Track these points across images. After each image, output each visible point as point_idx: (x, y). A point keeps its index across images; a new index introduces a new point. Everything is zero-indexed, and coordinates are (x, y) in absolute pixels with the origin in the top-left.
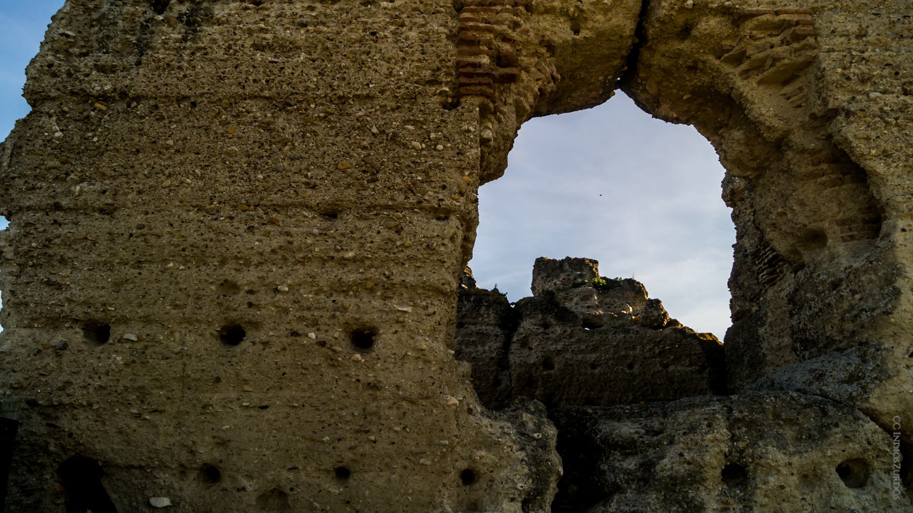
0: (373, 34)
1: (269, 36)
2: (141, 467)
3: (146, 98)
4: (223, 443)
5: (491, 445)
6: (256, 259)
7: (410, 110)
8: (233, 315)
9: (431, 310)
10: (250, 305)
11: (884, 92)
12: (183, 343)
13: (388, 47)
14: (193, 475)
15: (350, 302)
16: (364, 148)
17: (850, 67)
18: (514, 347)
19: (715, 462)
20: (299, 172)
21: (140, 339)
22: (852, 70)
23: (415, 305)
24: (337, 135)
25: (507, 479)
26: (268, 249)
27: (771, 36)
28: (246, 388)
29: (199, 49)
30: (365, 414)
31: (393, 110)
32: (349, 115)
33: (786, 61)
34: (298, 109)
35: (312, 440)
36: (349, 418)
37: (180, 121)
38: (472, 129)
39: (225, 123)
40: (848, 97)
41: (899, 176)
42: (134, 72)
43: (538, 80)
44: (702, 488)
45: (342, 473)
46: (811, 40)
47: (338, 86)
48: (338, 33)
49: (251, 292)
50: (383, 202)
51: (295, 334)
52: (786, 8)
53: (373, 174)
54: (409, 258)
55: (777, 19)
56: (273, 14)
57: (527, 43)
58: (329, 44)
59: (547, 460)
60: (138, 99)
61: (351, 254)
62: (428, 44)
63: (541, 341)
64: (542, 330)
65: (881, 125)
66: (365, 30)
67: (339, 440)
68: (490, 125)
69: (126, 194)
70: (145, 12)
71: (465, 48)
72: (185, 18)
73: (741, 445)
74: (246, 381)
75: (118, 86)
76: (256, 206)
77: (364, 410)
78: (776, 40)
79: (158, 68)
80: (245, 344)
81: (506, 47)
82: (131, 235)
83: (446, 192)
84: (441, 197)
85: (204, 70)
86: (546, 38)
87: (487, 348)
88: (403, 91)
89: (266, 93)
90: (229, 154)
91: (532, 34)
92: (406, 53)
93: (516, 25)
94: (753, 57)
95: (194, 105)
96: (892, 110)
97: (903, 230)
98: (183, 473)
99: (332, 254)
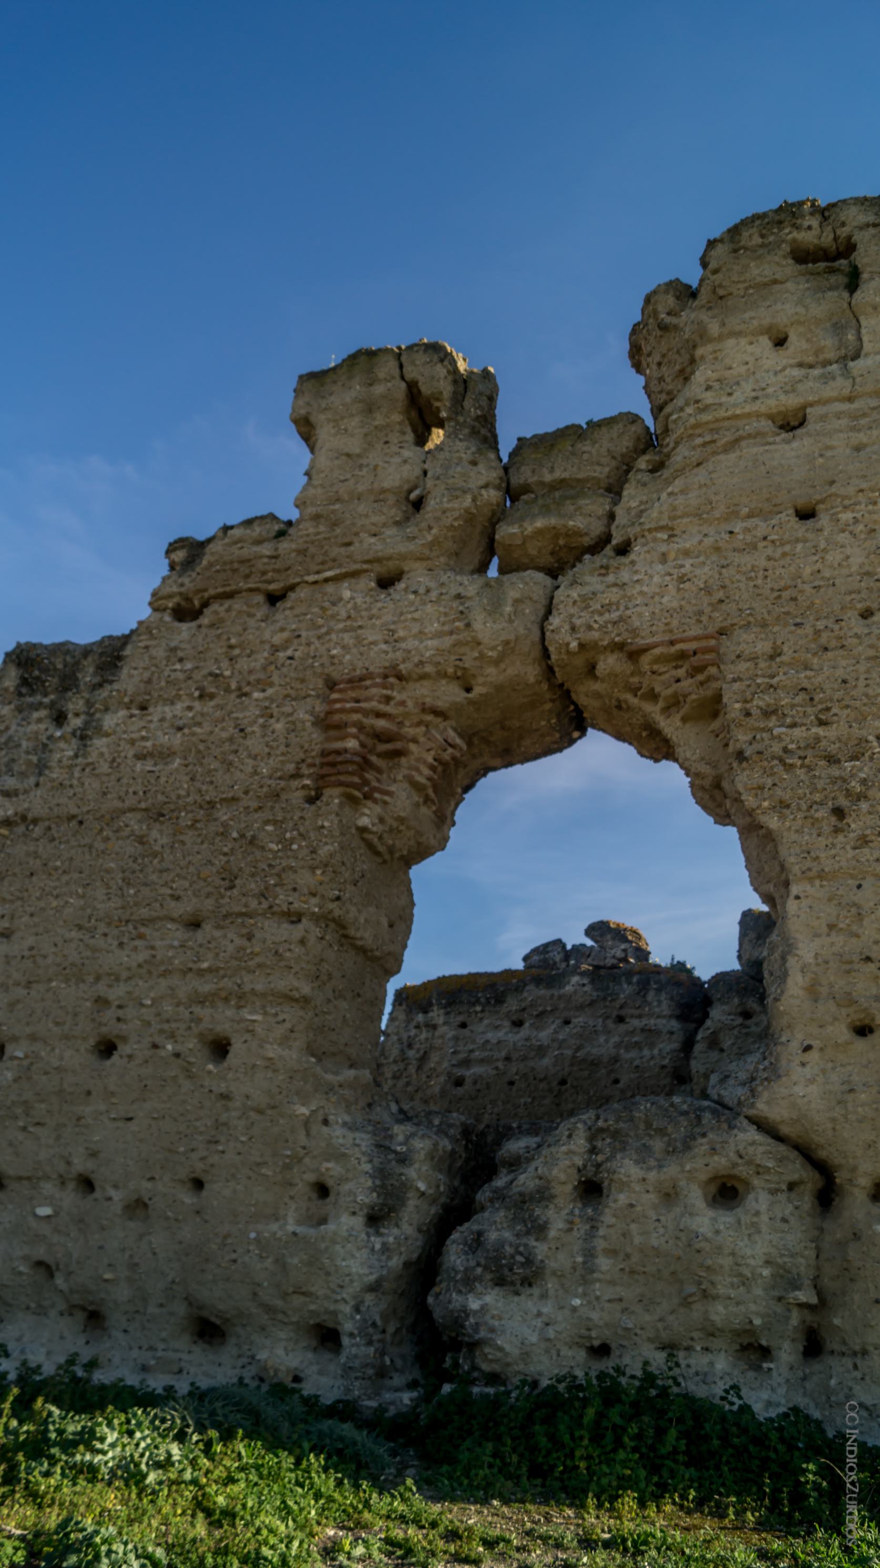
0: (242, 730)
1: (149, 744)
2: (29, 1178)
3: (42, 819)
4: (94, 1155)
5: (341, 1157)
6: (125, 974)
7: (272, 808)
8: (104, 1030)
9: (280, 1018)
10: (119, 1019)
11: (794, 725)
12: (61, 1058)
13: (255, 744)
14: (71, 1185)
15: (204, 1012)
16: (225, 854)
17: (752, 700)
18: (698, 1048)
19: (562, 1177)
20: (165, 884)
21: (26, 1057)
22: (755, 703)
23: (265, 1014)
24: (202, 843)
25: (350, 1192)
26: (134, 964)
27: (676, 667)
28: (114, 1100)
29: (88, 764)
30: (218, 1125)
31: (256, 811)
32: (216, 820)
33: (694, 697)
34: (170, 819)
35: (170, 1151)
36: (202, 1129)
37: (68, 842)
38: (326, 824)
39: (107, 839)
40: (749, 737)
41: (797, 831)
42: (32, 794)
43: (428, 750)
44: (551, 1206)
45: (198, 1184)
46: (713, 670)
47: (207, 791)
48: (211, 733)
49: (120, 1007)
50: (237, 909)
51: (155, 1046)
52: (686, 634)
53: (231, 881)
54: (259, 966)
55: (673, 650)
56: (155, 719)
57: (407, 715)
58: (201, 747)
59: (401, 1174)
60: (35, 821)
61: (205, 965)
62: (293, 734)
63: (737, 1038)
64: (739, 1020)
65: (779, 769)
66: (235, 727)
67: (193, 1150)
68: (367, 811)
69: (21, 917)
70: (47, 729)
71: (333, 733)
72: (79, 732)
73: (600, 1158)
74: (113, 1094)
75: (20, 809)
76: (127, 921)
77: (217, 1120)
78: (681, 672)
79: (53, 788)
80: (115, 1057)
81: (381, 723)
82: (23, 957)
83: (296, 895)
84: (291, 899)
85: (92, 785)
86: (427, 706)
87: (656, 1052)
88: (265, 789)
89: (143, 805)
90: (107, 871)
91: (410, 704)
92: (271, 747)
93: (388, 699)
94: (663, 694)
95: (81, 823)
96: (799, 748)
97: (797, 897)
98: (63, 1183)
99: (190, 965)
